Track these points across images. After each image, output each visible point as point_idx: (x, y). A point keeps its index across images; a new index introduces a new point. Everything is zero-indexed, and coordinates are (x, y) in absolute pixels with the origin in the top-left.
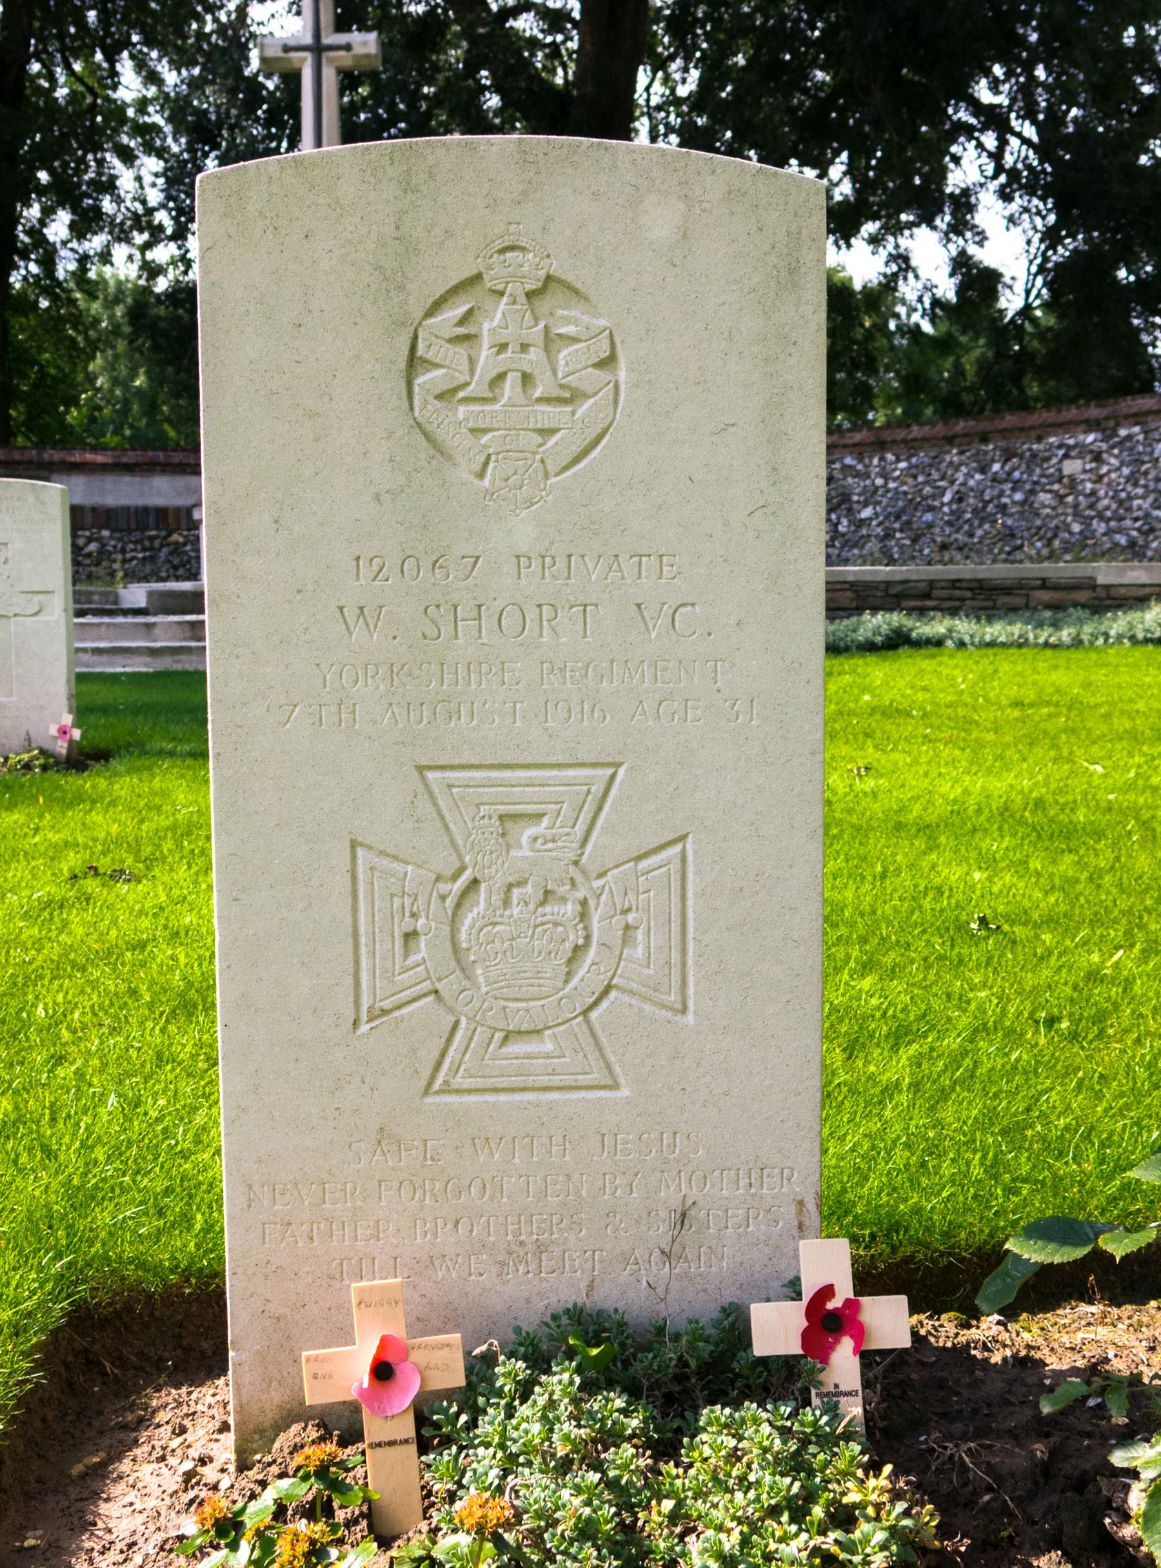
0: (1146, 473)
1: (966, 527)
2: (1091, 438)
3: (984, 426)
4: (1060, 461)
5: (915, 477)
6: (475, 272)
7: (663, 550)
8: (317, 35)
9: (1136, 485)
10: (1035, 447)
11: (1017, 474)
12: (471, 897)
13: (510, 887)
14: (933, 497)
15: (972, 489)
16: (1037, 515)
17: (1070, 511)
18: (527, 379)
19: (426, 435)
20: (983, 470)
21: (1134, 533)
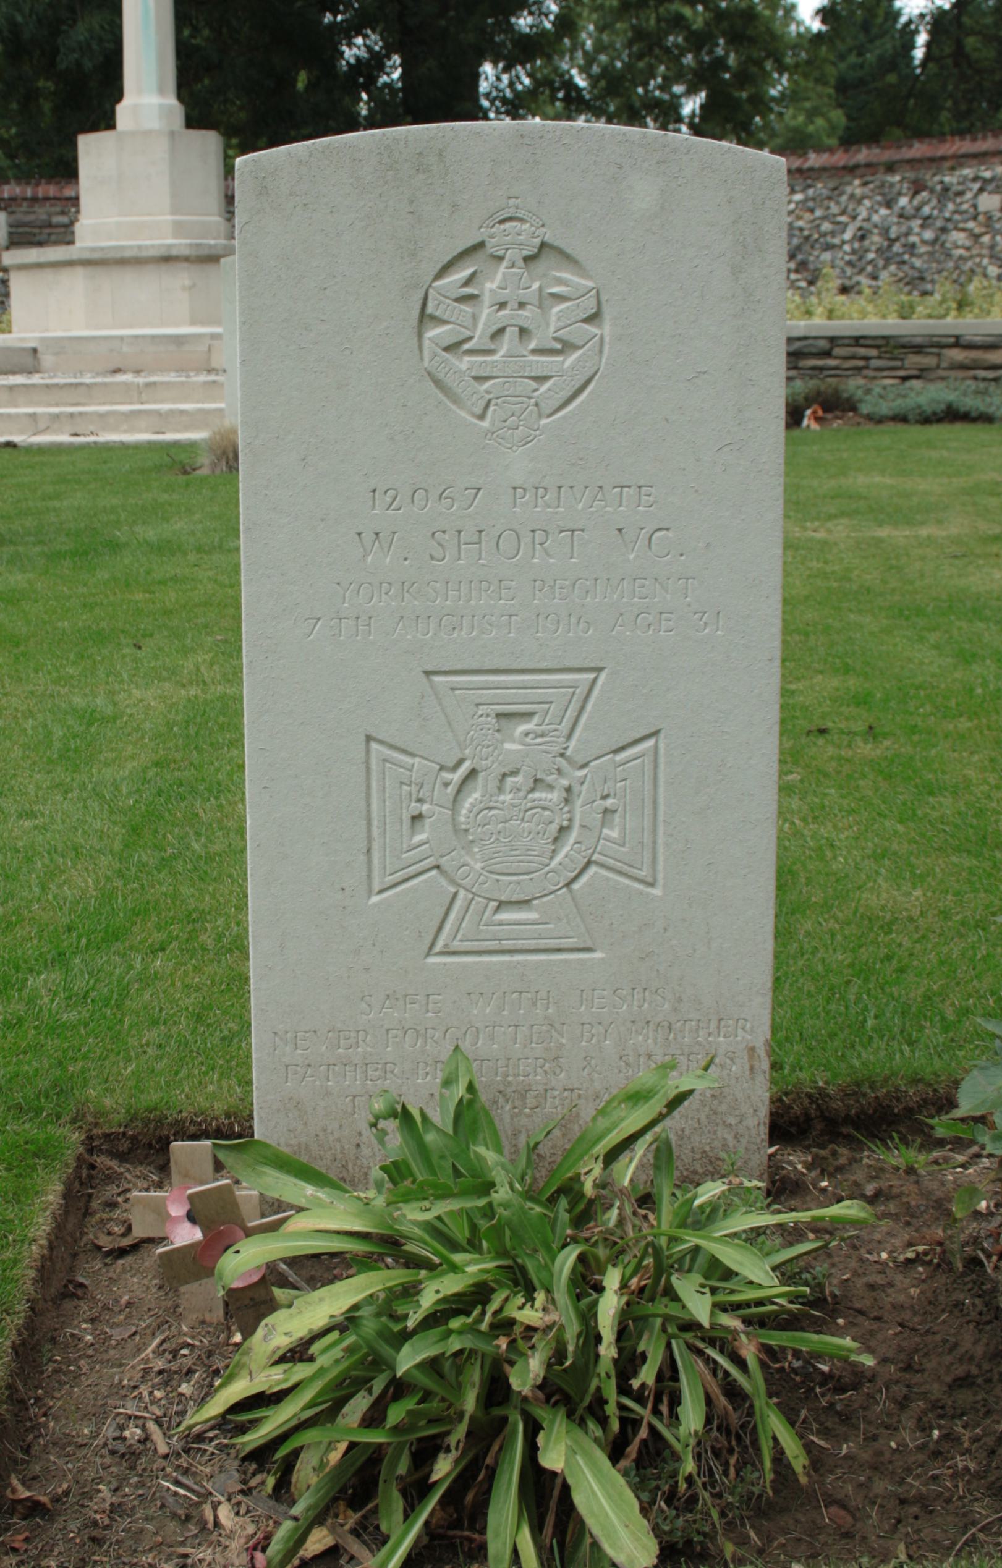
1: (869, 268)
4: (976, 196)
5: (812, 211)
6: (479, 240)
7: (641, 483)
11: (926, 210)
12: (470, 785)
13: (504, 775)
14: (833, 234)
15: (876, 226)
16: (949, 255)
17: (985, 252)
18: (523, 332)
19: (437, 383)
20: (889, 204)
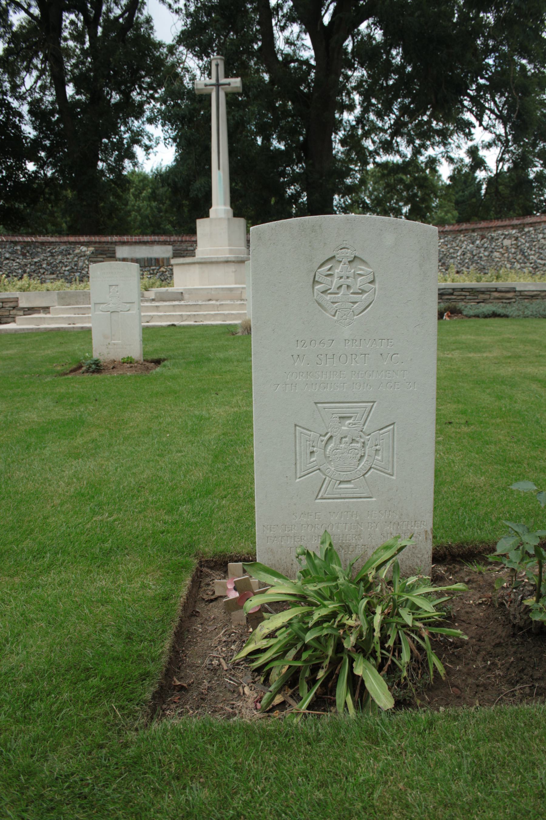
0: (535, 246)
2: (514, 231)
3: (473, 226)
5: (447, 245)
8: (217, 80)
9: (531, 250)
10: (493, 234)
11: (486, 245)
12: (330, 441)
13: (342, 438)
14: (454, 253)
18: (348, 287)
20: (473, 243)
21: (531, 269)
